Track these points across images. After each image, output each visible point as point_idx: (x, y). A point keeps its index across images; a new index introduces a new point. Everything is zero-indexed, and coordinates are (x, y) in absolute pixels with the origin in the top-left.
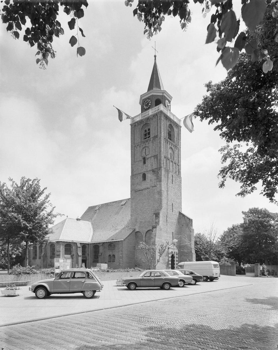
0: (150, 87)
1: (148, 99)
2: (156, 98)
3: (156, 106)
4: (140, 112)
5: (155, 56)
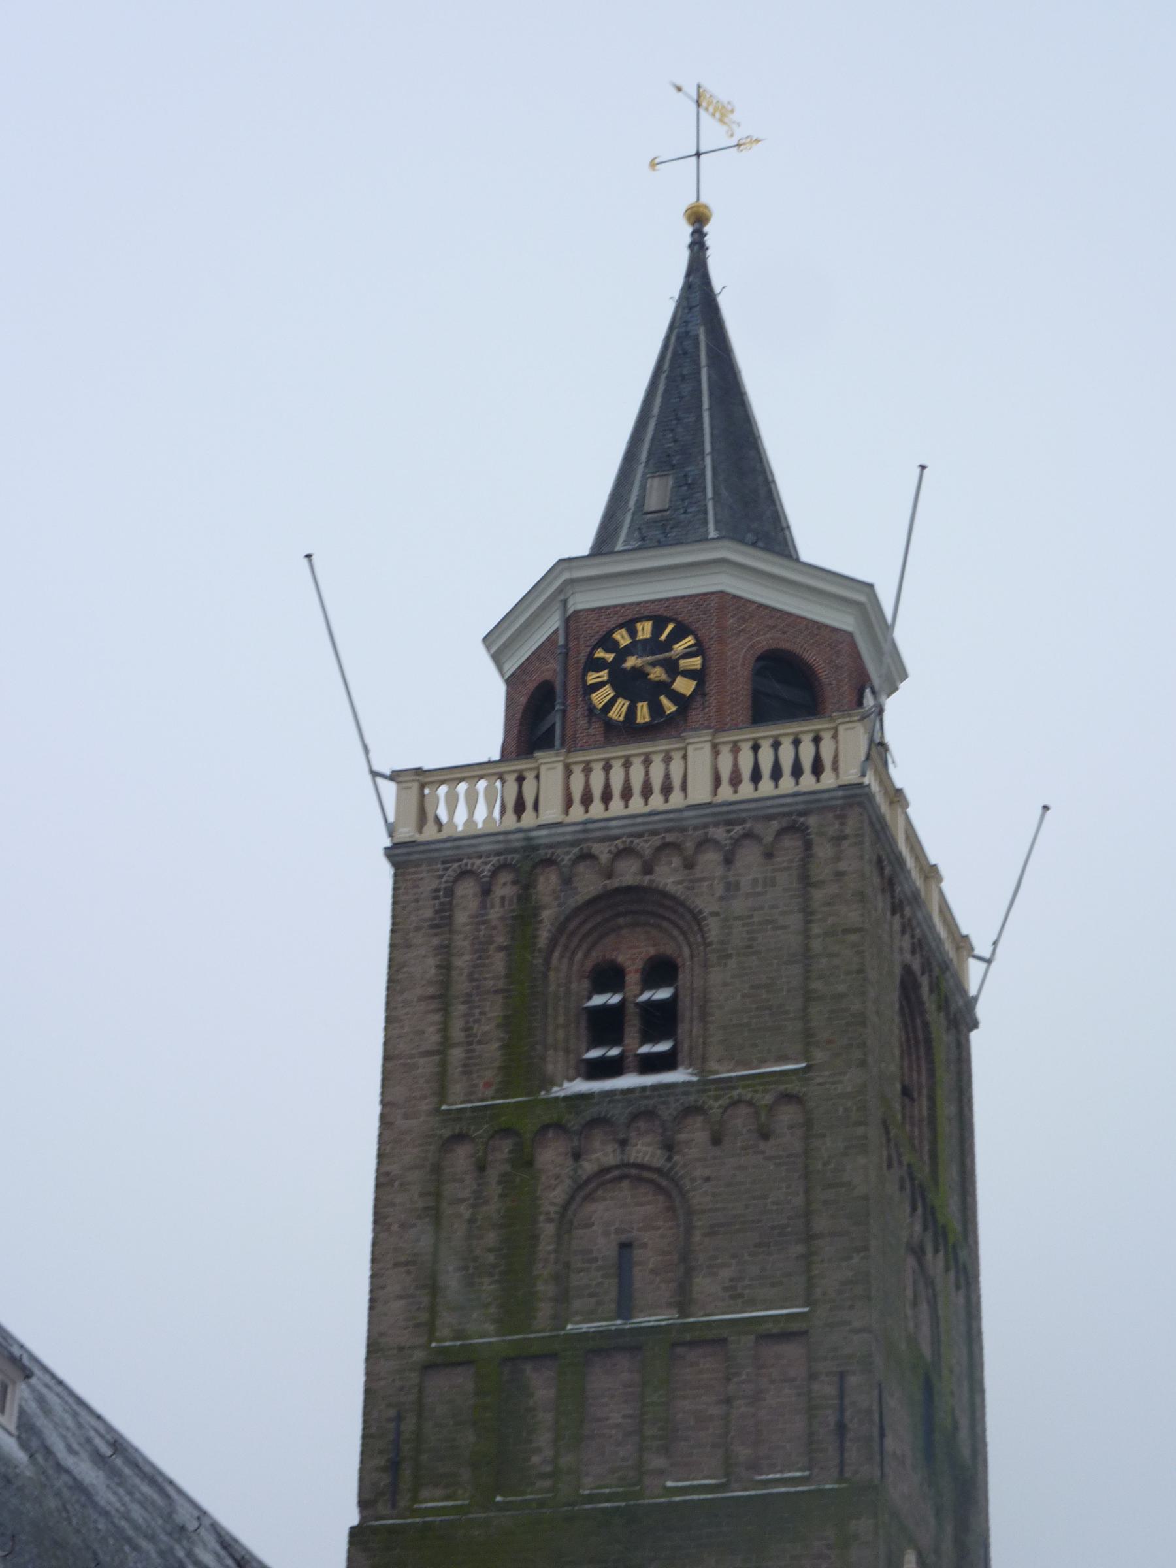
0: (631, 522)
1: (659, 623)
2: (765, 641)
4: (496, 756)
5: (698, 218)
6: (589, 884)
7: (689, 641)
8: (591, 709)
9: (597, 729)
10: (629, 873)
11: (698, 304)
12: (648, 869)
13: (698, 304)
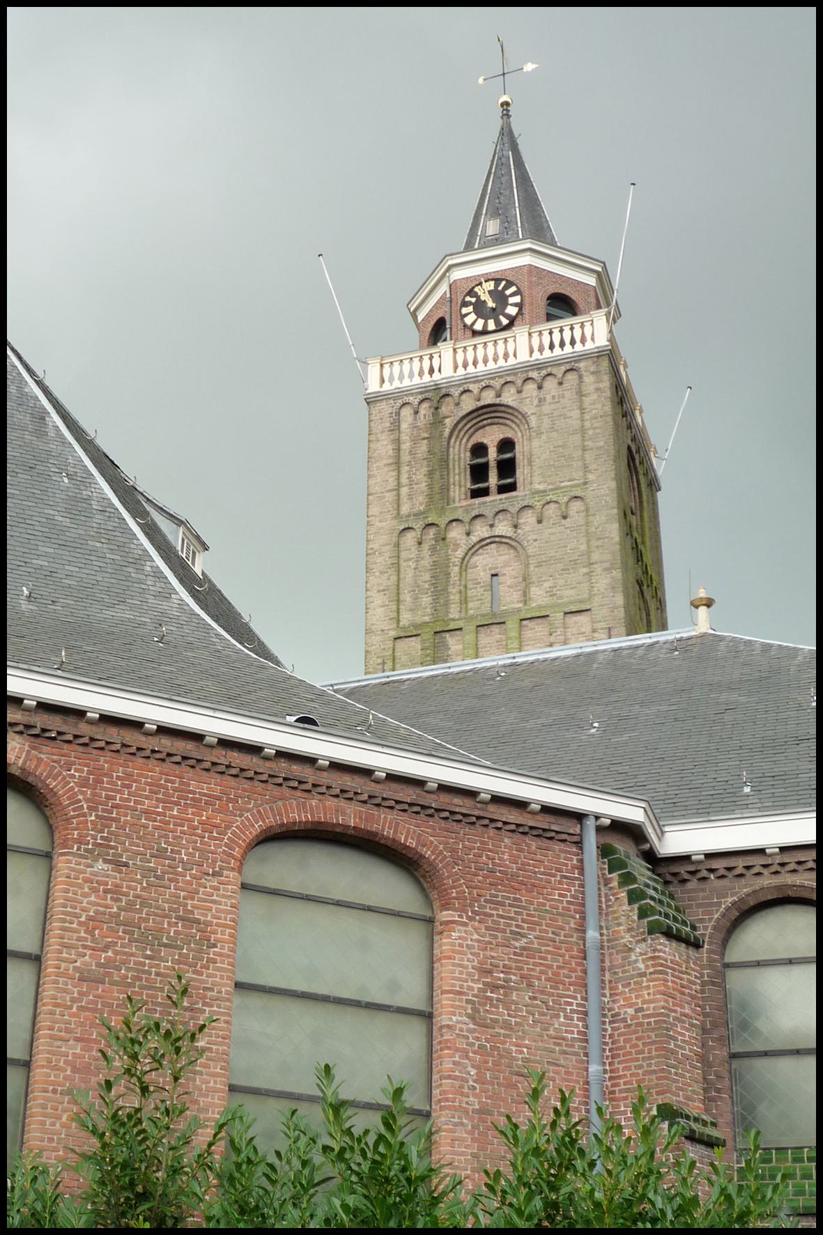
2: (552, 289)
3: (550, 317)
6: (468, 404)
7: (513, 289)
8: (465, 326)
9: (469, 333)
10: (489, 398)
11: (508, 138)
12: (498, 395)
13: (508, 138)
